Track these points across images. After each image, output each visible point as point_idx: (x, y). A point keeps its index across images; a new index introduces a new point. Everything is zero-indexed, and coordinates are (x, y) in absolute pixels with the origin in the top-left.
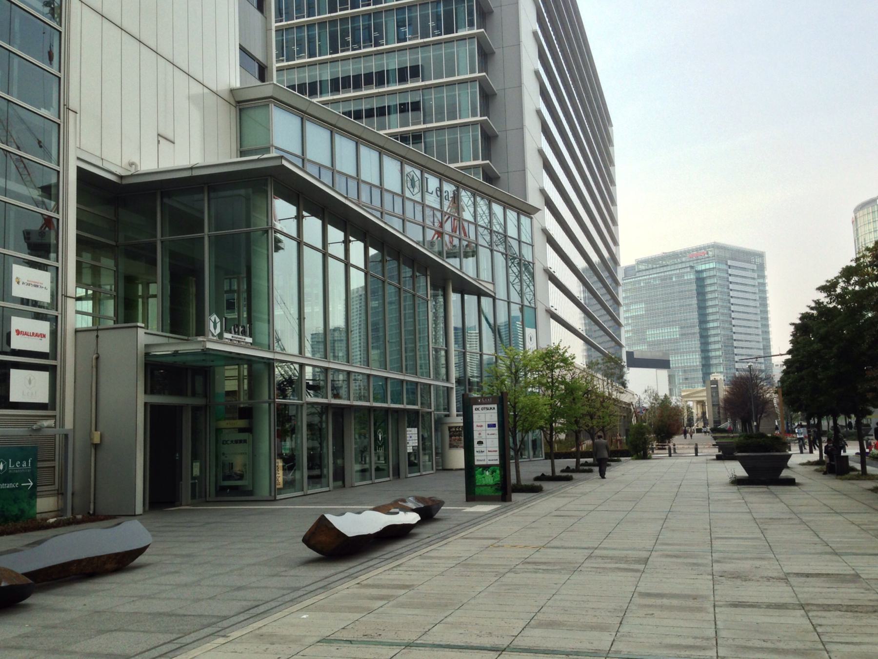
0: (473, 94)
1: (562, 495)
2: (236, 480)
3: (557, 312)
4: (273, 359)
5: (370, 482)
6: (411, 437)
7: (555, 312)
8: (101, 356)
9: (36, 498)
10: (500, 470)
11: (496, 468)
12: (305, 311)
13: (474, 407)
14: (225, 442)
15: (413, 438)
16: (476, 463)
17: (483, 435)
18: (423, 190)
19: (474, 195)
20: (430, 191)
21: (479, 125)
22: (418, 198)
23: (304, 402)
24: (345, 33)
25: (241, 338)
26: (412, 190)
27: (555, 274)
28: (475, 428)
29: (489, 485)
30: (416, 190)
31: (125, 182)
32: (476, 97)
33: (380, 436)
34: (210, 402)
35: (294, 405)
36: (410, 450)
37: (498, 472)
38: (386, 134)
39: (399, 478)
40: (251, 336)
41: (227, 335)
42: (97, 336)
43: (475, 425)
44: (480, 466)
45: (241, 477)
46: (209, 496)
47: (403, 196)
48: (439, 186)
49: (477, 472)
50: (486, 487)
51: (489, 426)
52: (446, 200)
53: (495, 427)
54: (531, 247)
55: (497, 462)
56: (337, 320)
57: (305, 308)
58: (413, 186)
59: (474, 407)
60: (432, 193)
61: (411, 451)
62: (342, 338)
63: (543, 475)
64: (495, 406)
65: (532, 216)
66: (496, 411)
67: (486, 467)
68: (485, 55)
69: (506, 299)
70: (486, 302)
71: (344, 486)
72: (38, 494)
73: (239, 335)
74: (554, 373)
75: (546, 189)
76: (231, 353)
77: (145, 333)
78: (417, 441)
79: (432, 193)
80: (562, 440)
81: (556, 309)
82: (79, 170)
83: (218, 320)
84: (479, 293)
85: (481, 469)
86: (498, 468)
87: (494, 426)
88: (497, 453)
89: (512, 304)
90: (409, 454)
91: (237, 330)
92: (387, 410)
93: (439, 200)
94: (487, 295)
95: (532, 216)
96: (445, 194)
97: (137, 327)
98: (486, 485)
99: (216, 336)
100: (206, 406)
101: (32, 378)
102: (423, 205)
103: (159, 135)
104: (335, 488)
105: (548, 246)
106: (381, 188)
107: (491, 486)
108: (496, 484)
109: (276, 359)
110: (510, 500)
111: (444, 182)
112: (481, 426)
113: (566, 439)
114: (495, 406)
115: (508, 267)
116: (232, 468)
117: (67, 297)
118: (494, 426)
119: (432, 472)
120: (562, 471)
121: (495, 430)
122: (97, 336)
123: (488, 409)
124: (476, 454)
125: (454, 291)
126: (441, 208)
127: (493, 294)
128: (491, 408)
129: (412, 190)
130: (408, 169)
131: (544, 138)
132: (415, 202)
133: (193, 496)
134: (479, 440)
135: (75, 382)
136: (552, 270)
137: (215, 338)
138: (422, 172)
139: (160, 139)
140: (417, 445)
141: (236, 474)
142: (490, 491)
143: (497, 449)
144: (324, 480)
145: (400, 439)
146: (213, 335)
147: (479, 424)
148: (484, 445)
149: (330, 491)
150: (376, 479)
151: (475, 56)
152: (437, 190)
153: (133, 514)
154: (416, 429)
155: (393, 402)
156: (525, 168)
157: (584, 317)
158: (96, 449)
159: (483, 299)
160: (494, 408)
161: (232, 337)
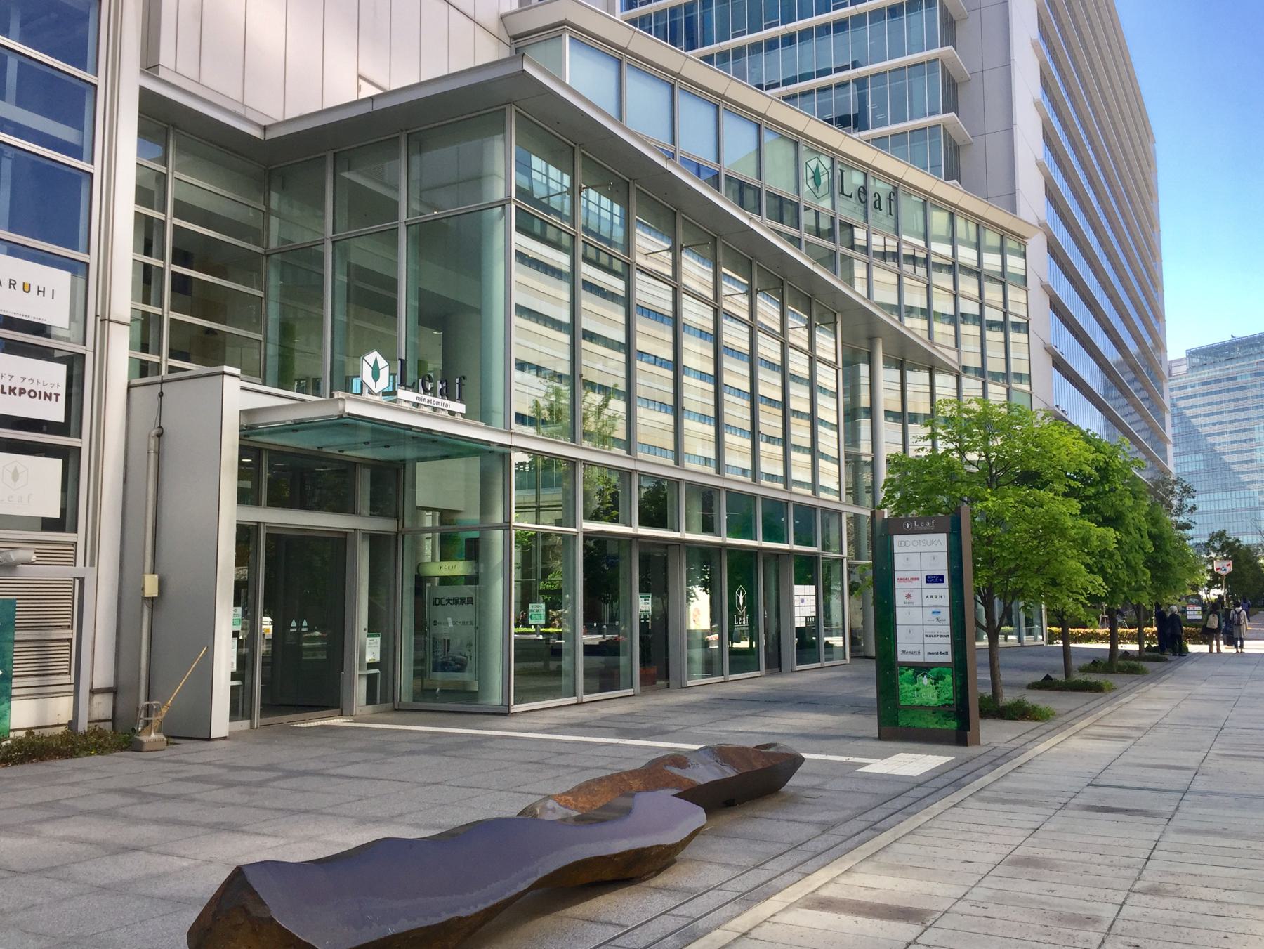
5: (721, 679)
6: (802, 601)
8: (165, 433)
9: (10, 701)
14: (437, 602)
15: (806, 603)
16: (901, 658)
29: (929, 707)
31: (270, 136)
33: (741, 598)
34: (403, 527)
35: (614, 539)
36: (800, 623)
37: (949, 679)
39: (780, 671)
40: (461, 400)
41: (403, 394)
42: (161, 395)
44: (910, 665)
45: (461, 666)
51: (929, 579)
52: (876, 208)
53: (943, 582)
60: (851, 197)
61: (804, 625)
67: (921, 668)
71: (668, 686)
72: (14, 692)
73: (435, 396)
77: (242, 388)
78: (814, 609)
79: (851, 197)
82: (144, 93)
83: (382, 363)
85: (911, 672)
87: (940, 579)
88: (948, 640)
90: (799, 629)
91: (429, 386)
92: (753, 553)
97: (223, 373)
98: (921, 706)
100: (397, 533)
101: (20, 470)
103: (360, 76)
107: (934, 710)
108: (944, 706)
109: (515, 446)
117: (110, 321)
118: (940, 579)
119: (843, 661)
121: (943, 590)
122: (161, 395)
125: (888, 363)
133: (371, 699)
135: (125, 481)
139: (361, 82)
142: (932, 723)
144: (565, 682)
145: (781, 606)
146: (371, 392)
155: (731, 533)
157: (1107, 426)
158: (152, 609)
159: (940, 379)
161: (418, 398)
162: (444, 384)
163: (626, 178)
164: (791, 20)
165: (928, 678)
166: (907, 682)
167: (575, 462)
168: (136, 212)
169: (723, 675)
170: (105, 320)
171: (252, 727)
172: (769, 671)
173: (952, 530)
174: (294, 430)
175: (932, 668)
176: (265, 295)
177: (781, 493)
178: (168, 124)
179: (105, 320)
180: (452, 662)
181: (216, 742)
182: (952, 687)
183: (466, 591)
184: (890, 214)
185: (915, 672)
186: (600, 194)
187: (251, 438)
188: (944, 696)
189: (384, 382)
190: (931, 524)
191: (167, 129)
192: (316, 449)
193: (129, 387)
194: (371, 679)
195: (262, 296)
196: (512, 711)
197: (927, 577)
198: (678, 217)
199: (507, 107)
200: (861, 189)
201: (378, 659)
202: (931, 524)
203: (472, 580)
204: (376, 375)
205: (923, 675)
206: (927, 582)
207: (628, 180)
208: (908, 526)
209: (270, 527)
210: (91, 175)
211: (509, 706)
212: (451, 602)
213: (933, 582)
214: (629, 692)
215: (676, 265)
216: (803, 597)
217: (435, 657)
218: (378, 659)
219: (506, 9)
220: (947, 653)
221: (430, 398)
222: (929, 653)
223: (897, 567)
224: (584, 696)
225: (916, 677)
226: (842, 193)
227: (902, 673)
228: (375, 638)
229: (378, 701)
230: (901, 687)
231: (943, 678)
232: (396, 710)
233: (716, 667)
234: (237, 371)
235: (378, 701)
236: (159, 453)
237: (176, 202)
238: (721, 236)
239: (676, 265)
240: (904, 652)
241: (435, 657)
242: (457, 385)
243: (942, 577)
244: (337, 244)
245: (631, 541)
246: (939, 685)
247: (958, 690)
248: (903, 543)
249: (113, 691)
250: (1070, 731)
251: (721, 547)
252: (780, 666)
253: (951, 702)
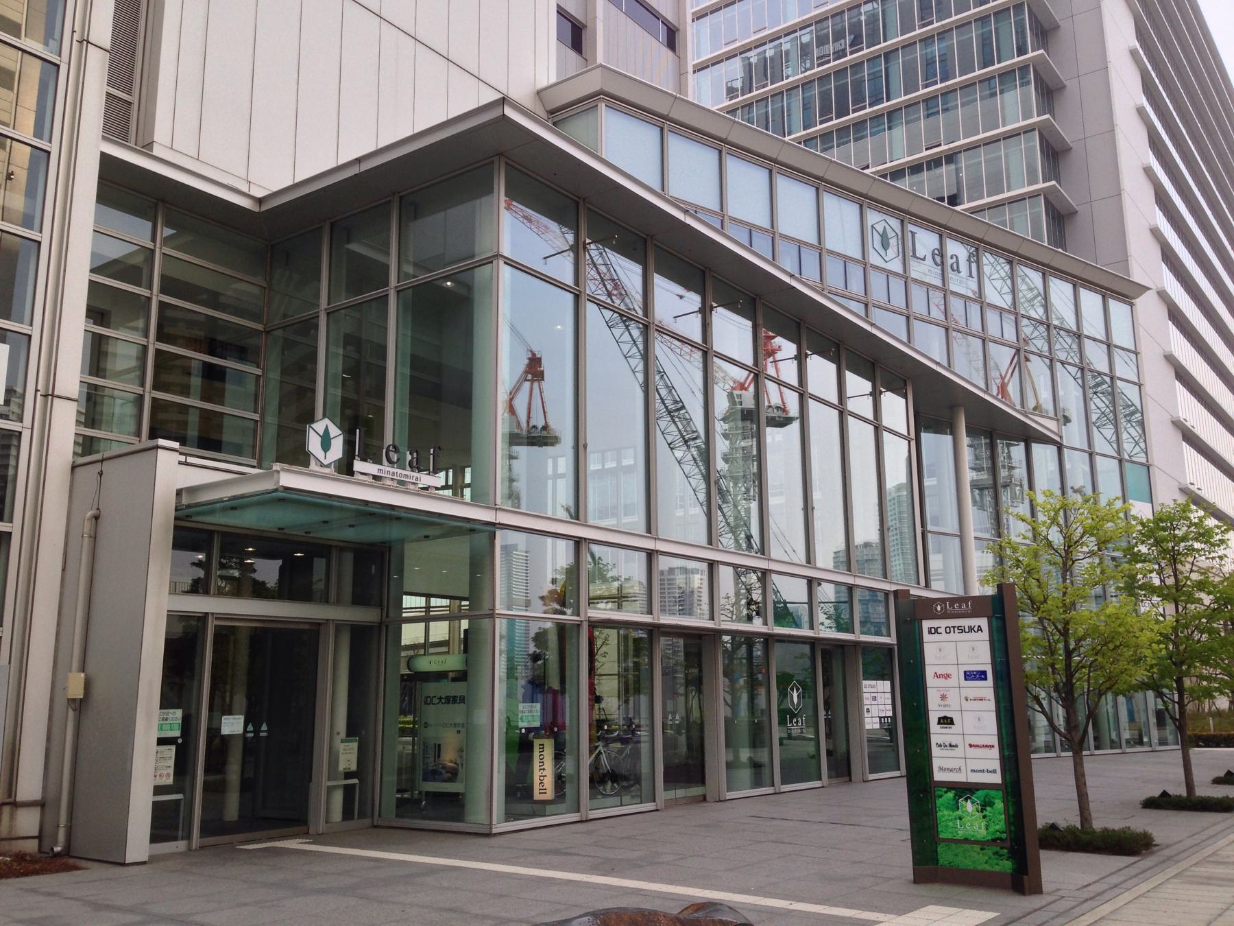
0: (1030, 151)
1: (1203, 870)
2: (445, 781)
3: (1203, 494)
4: (493, 524)
5: (770, 790)
6: (875, 699)
7: (1199, 492)
10: (1005, 802)
11: (993, 793)
12: (770, 503)
13: (926, 624)
16: (938, 776)
17: (953, 699)
18: (907, 253)
19: (1010, 262)
20: (920, 252)
21: (1042, 196)
22: (896, 266)
23: (582, 617)
24: (825, 97)
25: (406, 476)
26: (882, 252)
27: (1195, 430)
28: (930, 681)
29: (976, 842)
30: (892, 252)
31: (265, 208)
32: (1035, 154)
33: (795, 695)
34: (387, 616)
37: (999, 805)
39: (850, 780)
41: (359, 465)
42: (101, 474)
43: (929, 672)
44: (950, 786)
45: (453, 775)
46: (379, 816)
47: (864, 264)
48: (938, 247)
49: (939, 802)
50: (967, 846)
51: (969, 676)
52: (953, 270)
53: (985, 679)
54: (1133, 356)
55: (997, 779)
56: (866, 530)
57: (770, 499)
58: (885, 244)
59: (926, 624)
62: (876, 557)
63: (1165, 794)
64: (983, 622)
65: (1133, 301)
66: (985, 635)
67: (964, 790)
68: (1049, 92)
69: (1086, 448)
70: (1043, 455)
74: (1179, 566)
75: (1169, 291)
76: (366, 503)
78: (890, 707)
79: (924, 259)
80: (1223, 711)
81: (1199, 489)
83: (334, 431)
84: (1029, 437)
85: (951, 795)
86: (1000, 794)
87: (982, 675)
88: (995, 753)
89: (1098, 458)
91: (395, 457)
93: (940, 272)
94: (1045, 440)
95: (1133, 301)
96: (950, 261)
97: (158, 447)
98: (966, 841)
99: (328, 466)
100: (380, 623)
102: (906, 278)
104: (672, 804)
105: (1178, 384)
106: (820, 248)
107: (983, 844)
108: (994, 840)
109: (500, 524)
110: (1037, 889)
111: (948, 240)
112: (947, 676)
113: (1230, 708)
114: (983, 622)
115: (1088, 400)
116: (439, 756)
118: (982, 675)
120: (1217, 781)
121: (986, 689)
123: (963, 631)
124: (935, 751)
126: (944, 285)
127: (1058, 439)
128: (971, 629)
129: (883, 255)
130: (873, 217)
131: (1161, 214)
132: (889, 273)
133: (347, 813)
134: (942, 715)
135: (64, 570)
136: (1188, 424)
137: (327, 470)
138: (902, 222)
140: (890, 714)
141: (444, 767)
142: (978, 860)
143: (994, 741)
147: (940, 671)
148: (956, 728)
149: (823, 787)
150: (783, 784)
151: (1031, 99)
152: (933, 254)
153: (123, 862)
154: (887, 684)
156: (1127, 256)
159: (1036, 448)
160: (980, 629)
161: (380, 470)
162: (415, 455)
163: (641, 234)
164: (880, 101)
165: (973, 803)
166: (947, 808)
167: (712, 564)
168: (91, 282)
169: (654, 801)
170: (49, 395)
171: (190, 849)
172: (834, 781)
173: (994, 613)
174: (234, 508)
175: (978, 790)
176: (263, 373)
177: (800, 568)
178: (157, 199)
179: (49, 395)
180: (443, 771)
181: (130, 868)
182: (1003, 816)
183: (458, 689)
184: (971, 276)
185: (956, 795)
186: (644, 263)
187: (194, 519)
188: (993, 828)
189: (337, 450)
190: (967, 606)
191: (156, 205)
192: (277, 530)
193: (74, 467)
194: (348, 791)
195: (260, 374)
196: (494, 831)
197: (965, 672)
198: (649, 243)
199: (496, 159)
200: (936, 252)
201: (354, 767)
202: (967, 606)
203: (462, 676)
204: (326, 444)
205: (966, 800)
206: (966, 679)
207: (644, 236)
208: (939, 608)
209: (219, 617)
210: (39, 243)
211: (491, 824)
212: (443, 701)
213: (972, 679)
214: (817, 784)
215: (706, 327)
216: (875, 695)
217: (425, 764)
218: (354, 767)
219: (543, 83)
220: (995, 771)
221: (395, 470)
222: (972, 771)
223: (927, 661)
224: (727, 794)
225: (957, 802)
226: (914, 256)
227: (941, 796)
228: (351, 744)
229: (356, 816)
230: (939, 814)
231: (991, 804)
232: (375, 827)
233: (766, 777)
234: (176, 445)
235: (356, 816)
236: (94, 538)
237: (163, 278)
238: (760, 296)
239: (706, 327)
240: (941, 769)
241: (425, 764)
242: (432, 456)
243: (984, 673)
244: (331, 315)
245: (652, 630)
246: (987, 813)
247: (1011, 819)
248: (933, 630)
249: (41, 804)
250: (1172, 871)
251: (856, 644)
252: (849, 774)
253: (1004, 836)
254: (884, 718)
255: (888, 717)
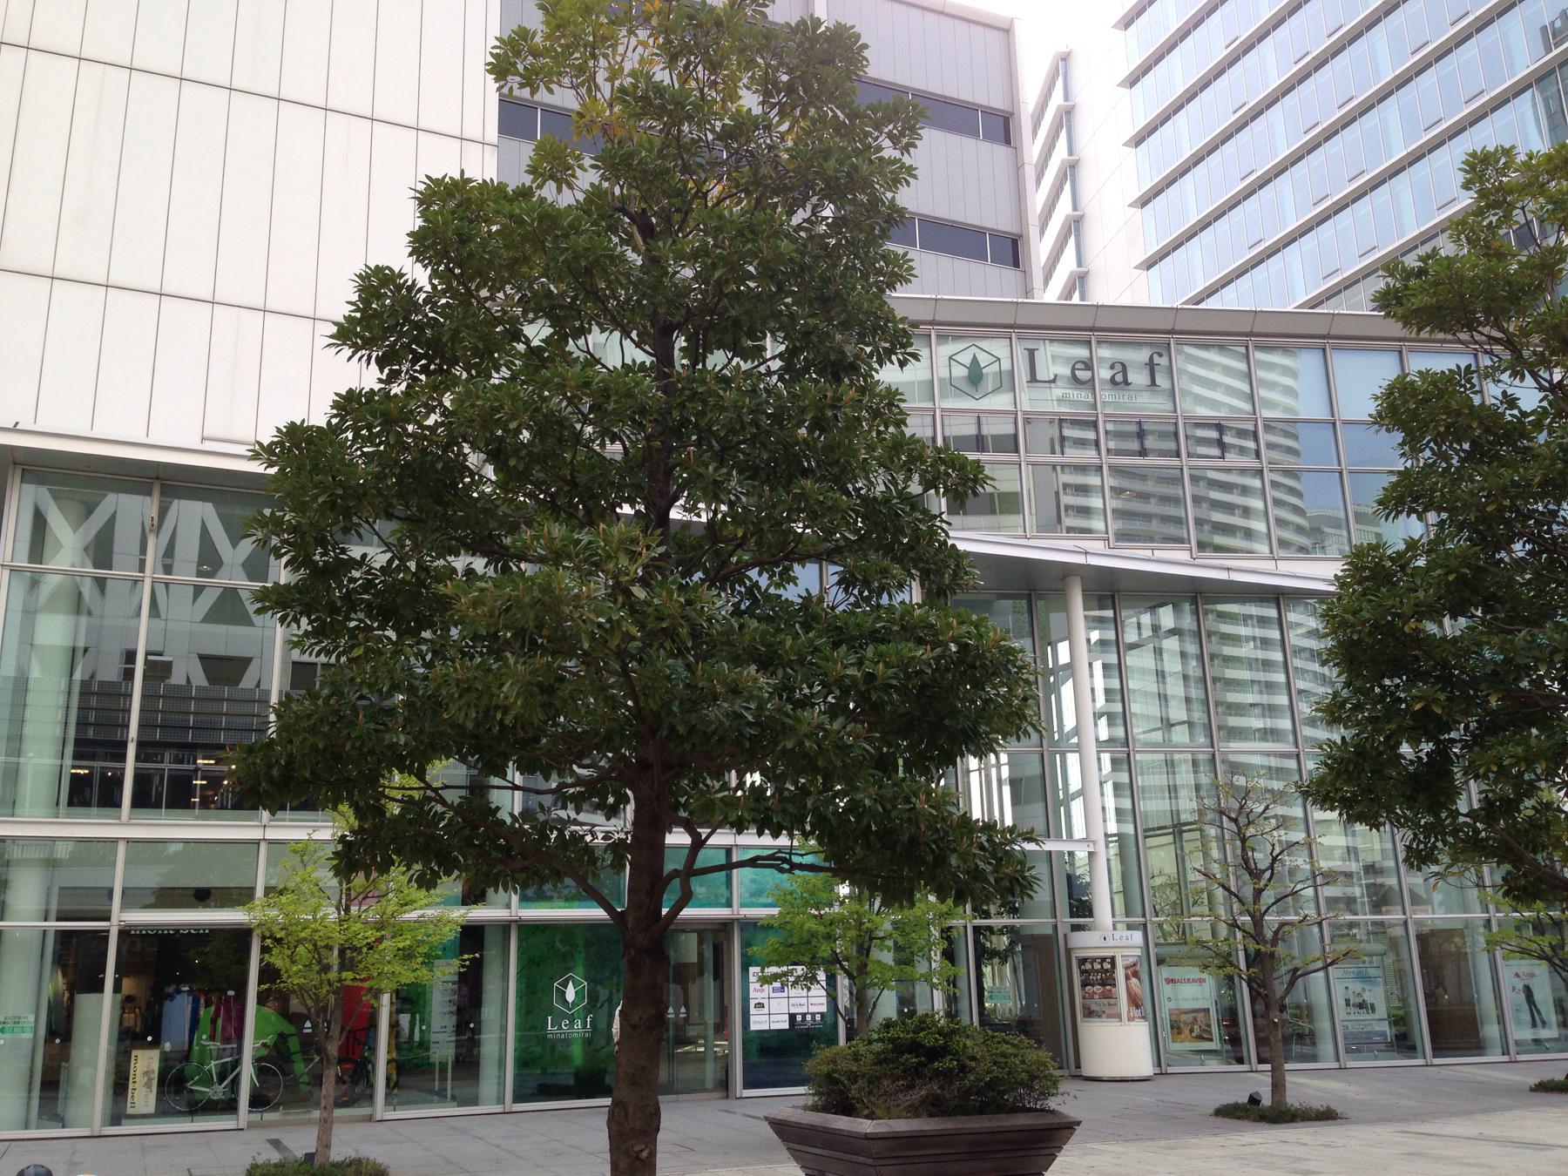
38: (1183, 303)
140: (824, 1009)
226: (1033, 379)
254: (804, 1015)
255: (813, 1015)
